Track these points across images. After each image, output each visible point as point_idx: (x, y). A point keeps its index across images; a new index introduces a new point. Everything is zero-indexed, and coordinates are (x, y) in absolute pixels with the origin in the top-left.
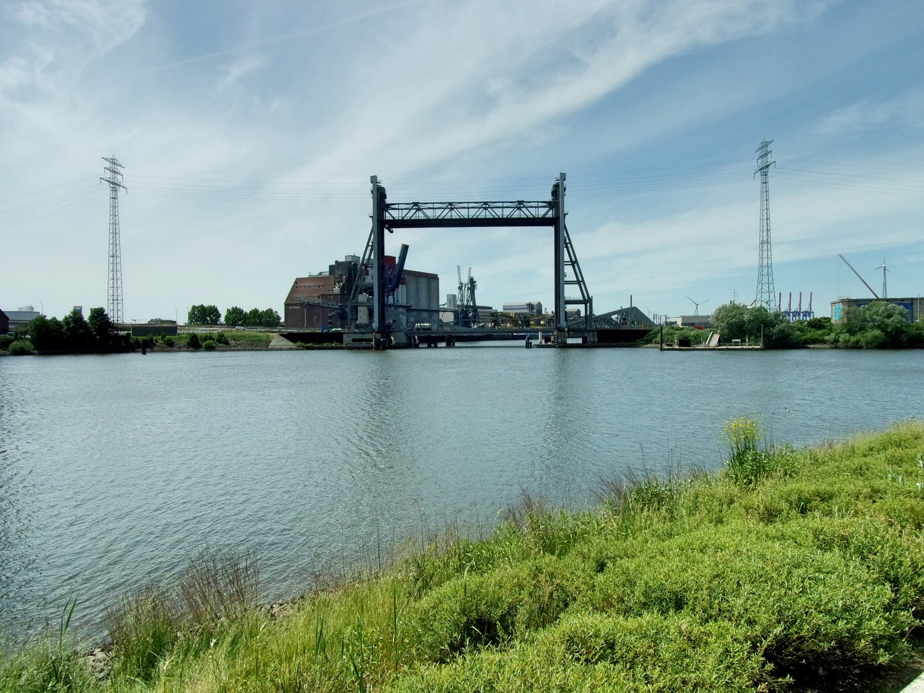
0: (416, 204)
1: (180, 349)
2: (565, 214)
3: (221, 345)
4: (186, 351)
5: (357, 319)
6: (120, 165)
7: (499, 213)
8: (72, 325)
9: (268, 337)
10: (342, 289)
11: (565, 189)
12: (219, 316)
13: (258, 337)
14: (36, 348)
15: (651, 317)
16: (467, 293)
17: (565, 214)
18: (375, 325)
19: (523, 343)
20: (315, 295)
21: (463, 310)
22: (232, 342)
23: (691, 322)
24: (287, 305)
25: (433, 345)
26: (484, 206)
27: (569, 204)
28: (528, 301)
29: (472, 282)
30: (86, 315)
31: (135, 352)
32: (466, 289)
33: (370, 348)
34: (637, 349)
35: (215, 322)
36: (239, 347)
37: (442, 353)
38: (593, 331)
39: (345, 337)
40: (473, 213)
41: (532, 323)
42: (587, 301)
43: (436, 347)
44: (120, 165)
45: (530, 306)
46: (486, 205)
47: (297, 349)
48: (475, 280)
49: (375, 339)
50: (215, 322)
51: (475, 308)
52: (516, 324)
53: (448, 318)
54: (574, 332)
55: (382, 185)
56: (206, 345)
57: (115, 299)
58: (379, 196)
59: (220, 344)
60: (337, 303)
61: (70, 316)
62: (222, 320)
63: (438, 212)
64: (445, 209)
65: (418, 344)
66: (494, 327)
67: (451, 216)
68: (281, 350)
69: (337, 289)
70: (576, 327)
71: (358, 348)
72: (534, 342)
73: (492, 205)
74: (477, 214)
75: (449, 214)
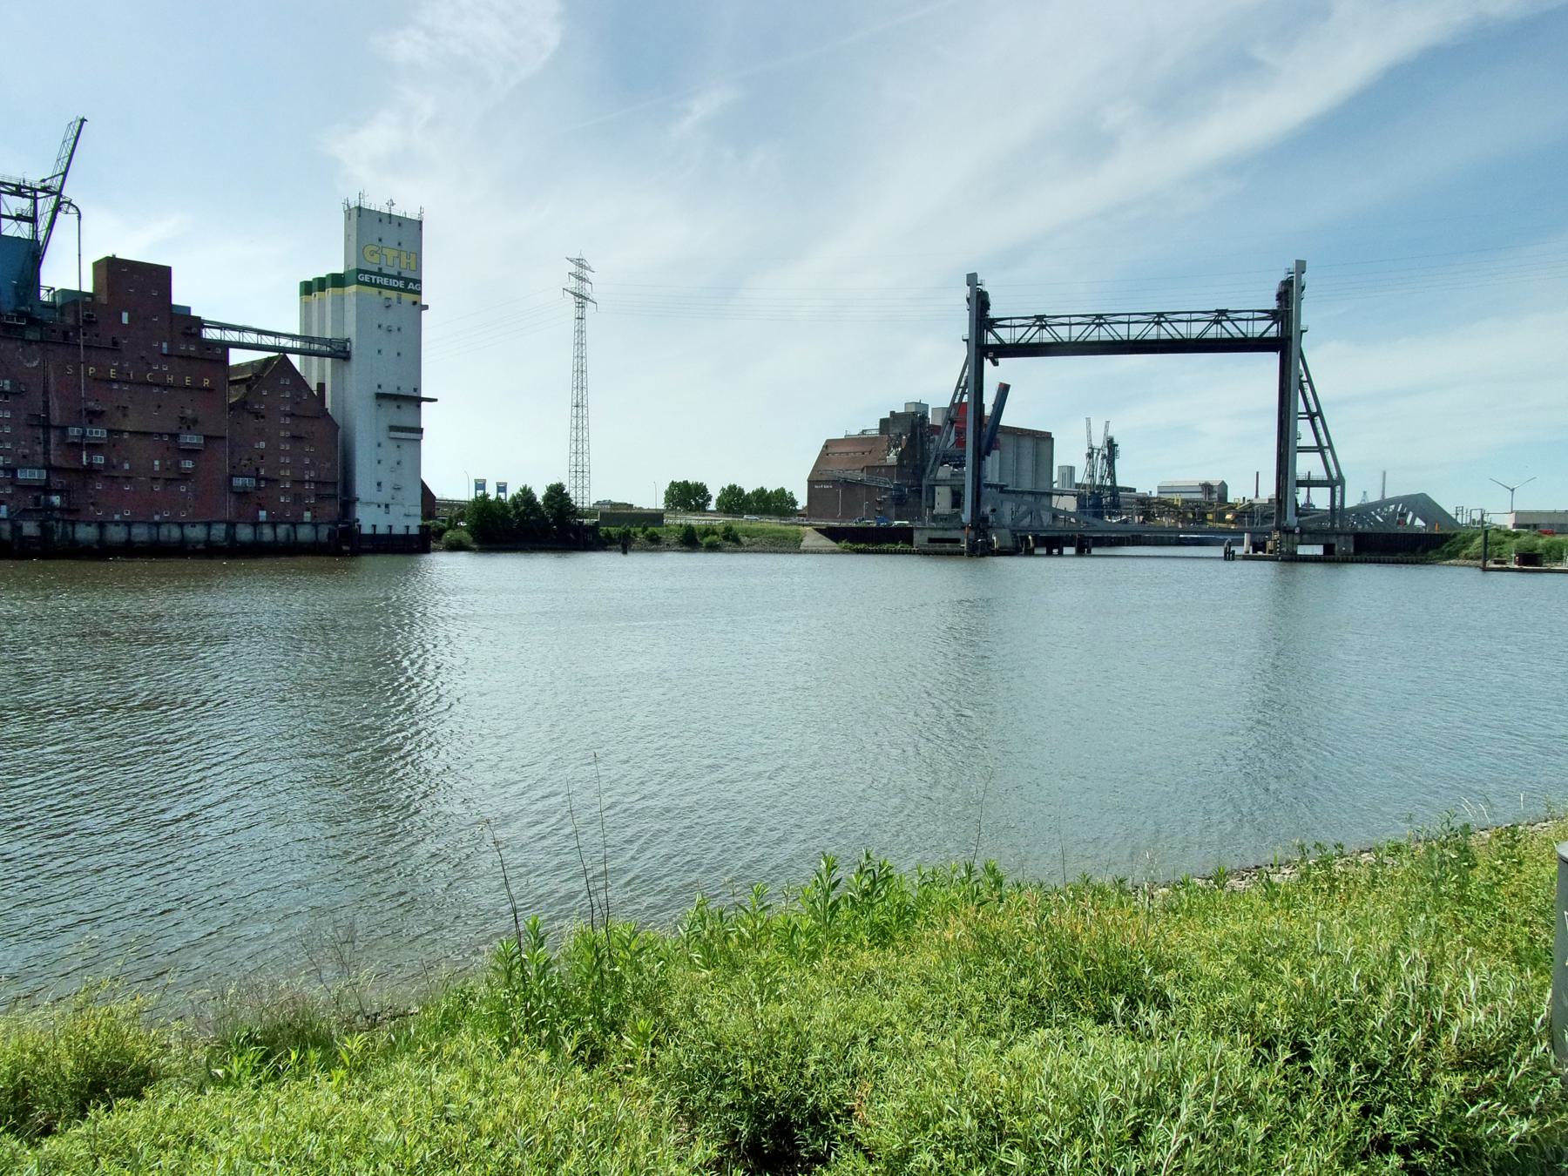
0: (1040, 318)
1: (669, 548)
2: (1302, 332)
3: (729, 543)
4: (678, 551)
5: (933, 508)
6: (589, 269)
7: (1183, 330)
8: (523, 508)
9: (798, 533)
10: (900, 457)
11: (1303, 288)
12: (710, 498)
13: (782, 532)
14: (475, 541)
15: (1451, 511)
16: (1100, 465)
17: (1302, 332)
18: (966, 517)
19: (1219, 551)
20: (857, 466)
21: (1094, 493)
22: (744, 539)
23: (1530, 522)
24: (811, 482)
25: (1055, 551)
26: (1097, 321)
27: (1309, 315)
28: (1203, 480)
29: (1111, 445)
30: (540, 494)
31: (605, 550)
32: (1100, 457)
33: (961, 554)
34: (1429, 567)
35: (701, 508)
36: (755, 547)
37: (1066, 568)
38: (1346, 534)
39: (916, 535)
40: (1136, 332)
41: (1210, 517)
42: (1334, 483)
43: (1061, 554)
44: (589, 269)
45: (1207, 488)
46: (1099, 320)
47: (843, 553)
48: (1116, 442)
49: (969, 540)
50: (701, 508)
51: (1114, 490)
52: (1184, 520)
53: (1069, 504)
54: (1310, 536)
55: (985, 289)
56: (707, 544)
57: (580, 471)
58: (980, 305)
59: (729, 541)
60: (891, 480)
61: (518, 495)
62: (712, 506)
63: (1019, 332)
64: (1089, 324)
65: (1033, 550)
66: (1143, 522)
67: (1158, 335)
68: (819, 552)
69: (892, 458)
70: (1314, 526)
71: (937, 553)
72: (1239, 551)
73: (1171, 317)
74: (1085, 334)
75: (1037, 335)
